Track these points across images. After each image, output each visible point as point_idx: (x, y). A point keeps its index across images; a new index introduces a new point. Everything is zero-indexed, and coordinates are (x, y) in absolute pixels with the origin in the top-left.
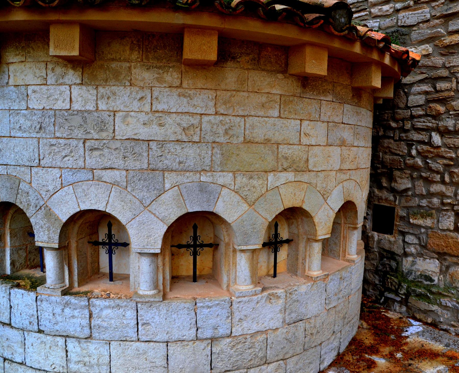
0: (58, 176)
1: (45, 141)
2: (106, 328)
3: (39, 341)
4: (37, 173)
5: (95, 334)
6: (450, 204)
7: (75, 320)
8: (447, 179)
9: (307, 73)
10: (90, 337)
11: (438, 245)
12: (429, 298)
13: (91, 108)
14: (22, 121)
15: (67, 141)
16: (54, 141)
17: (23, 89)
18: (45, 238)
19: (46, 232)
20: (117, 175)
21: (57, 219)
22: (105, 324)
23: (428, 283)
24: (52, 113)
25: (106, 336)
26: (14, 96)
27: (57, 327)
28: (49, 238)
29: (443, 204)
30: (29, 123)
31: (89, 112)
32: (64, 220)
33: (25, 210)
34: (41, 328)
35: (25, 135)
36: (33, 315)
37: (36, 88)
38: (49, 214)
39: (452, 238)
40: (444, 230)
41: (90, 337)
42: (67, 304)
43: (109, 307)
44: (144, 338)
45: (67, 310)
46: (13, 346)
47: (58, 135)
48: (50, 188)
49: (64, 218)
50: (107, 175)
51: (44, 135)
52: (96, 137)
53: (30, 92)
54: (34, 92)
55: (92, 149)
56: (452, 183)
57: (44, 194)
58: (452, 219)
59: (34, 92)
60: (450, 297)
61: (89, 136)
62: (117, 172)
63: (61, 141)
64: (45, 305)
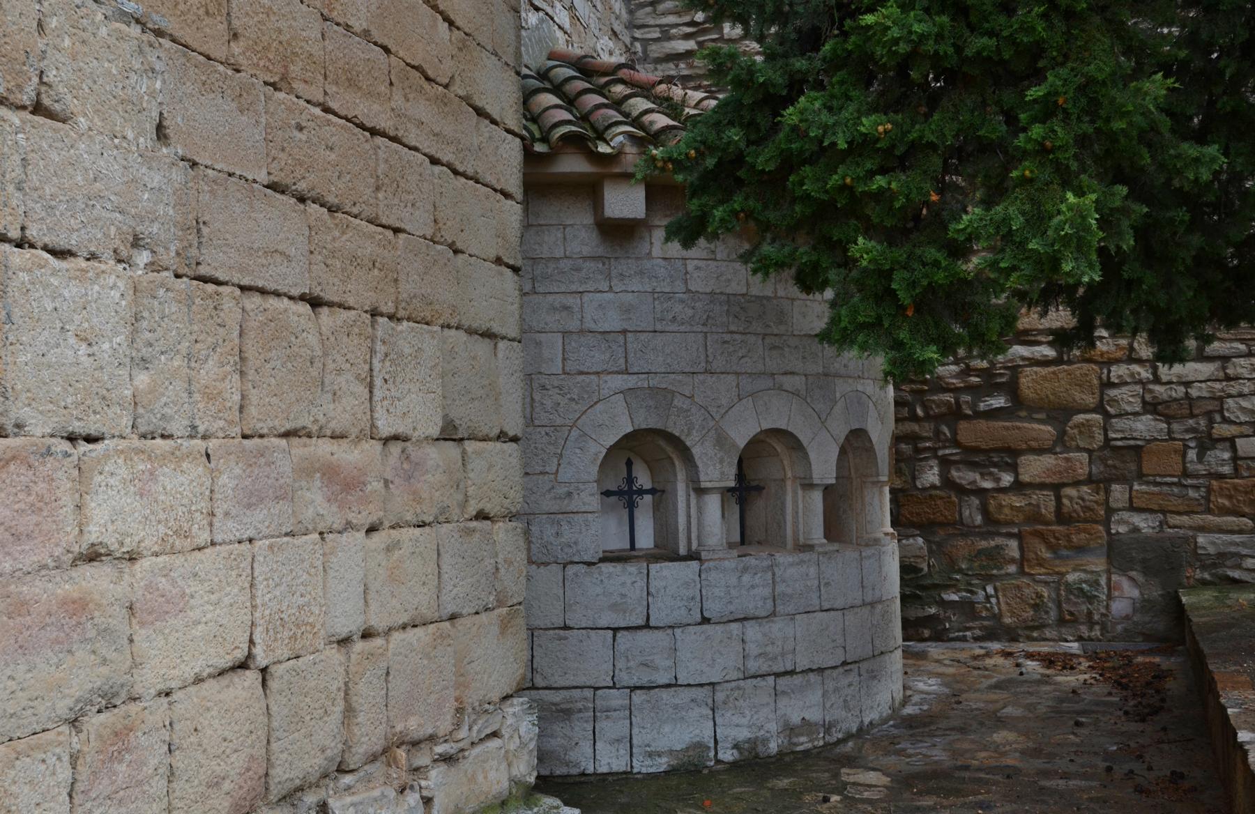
0: (734, 384)
1: (716, 337)
2: (791, 596)
3: (703, 636)
4: (703, 382)
5: (780, 608)
6: (929, 448)
7: (756, 591)
8: (920, 412)
9: (610, 218)
10: (774, 614)
11: (918, 514)
12: (919, 597)
13: (770, 294)
14: (678, 308)
15: (743, 337)
16: (727, 337)
17: (679, 263)
18: (716, 475)
19: (718, 467)
20: (797, 382)
21: (734, 445)
22: (789, 591)
23: (913, 576)
24: (723, 298)
25: (790, 609)
26: (662, 272)
27: (732, 608)
28: (722, 473)
29: (917, 451)
30: (690, 312)
31: (768, 298)
32: (742, 446)
33: (683, 438)
34: (706, 615)
35: (683, 328)
36: (693, 598)
37: (701, 263)
38: (721, 440)
39: (941, 498)
40: (924, 489)
41: (774, 614)
42: (745, 569)
43: (791, 565)
44: (826, 606)
45: (746, 578)
46: (652, 661)
47: (733, 328)
48: (724, 402)
49: (742, 444)
50: (788, 382)
51: (714, 329)
52: (776, 331)
53: (690, 268)
54: (697, 268)
55: (773, 348)
56: (928, 417)
57: (713, 410)
58: (936, 470)
59: (697, 268)
60: (954, 586)
61: (769, 331)
62: (797, 378)
63: (737, 336)
64: (713, 576)
